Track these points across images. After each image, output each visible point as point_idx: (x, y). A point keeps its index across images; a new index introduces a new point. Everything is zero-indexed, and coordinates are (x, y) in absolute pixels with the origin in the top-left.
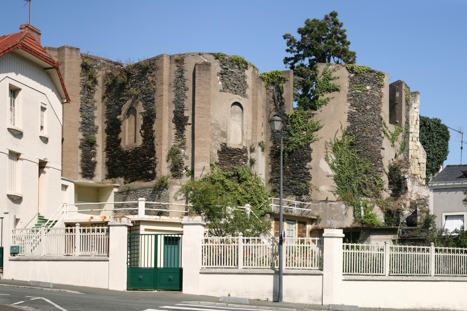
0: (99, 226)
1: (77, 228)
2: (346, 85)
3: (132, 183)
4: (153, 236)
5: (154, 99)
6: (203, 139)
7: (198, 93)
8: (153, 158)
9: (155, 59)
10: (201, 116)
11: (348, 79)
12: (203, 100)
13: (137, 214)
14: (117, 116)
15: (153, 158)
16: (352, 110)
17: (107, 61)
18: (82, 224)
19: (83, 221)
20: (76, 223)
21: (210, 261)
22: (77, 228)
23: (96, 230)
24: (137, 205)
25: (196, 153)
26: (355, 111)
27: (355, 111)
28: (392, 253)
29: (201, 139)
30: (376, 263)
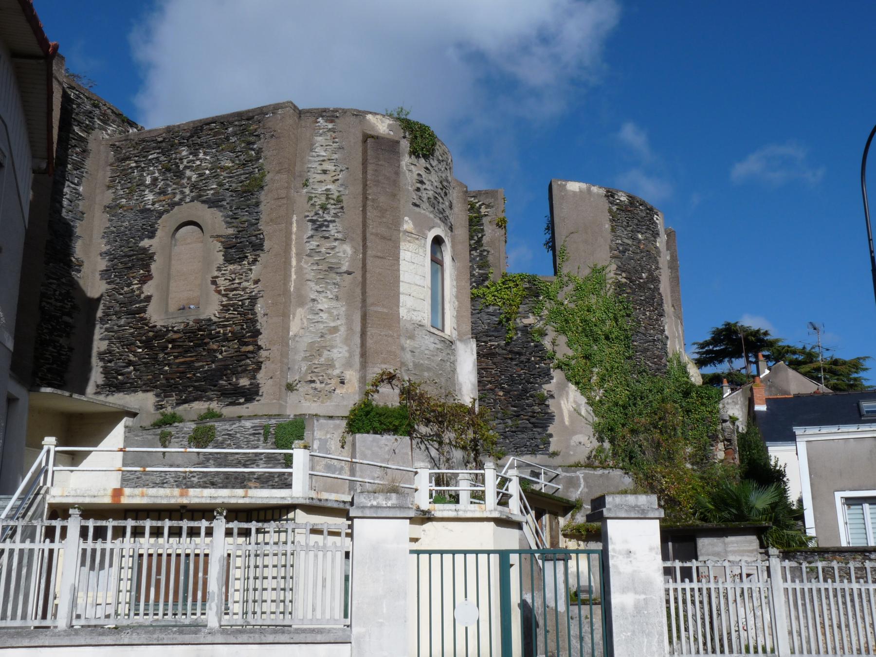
0: (249, 521)
1: (74, 524)
2: (607, 226)
3: (181, 408)
4: (495, 559)
5: (257, 204)
6: (385, 310)
7: (373, 200)
8: (251, 348)
9: (262, 112)
10: (379, 254)
11: (608, 216)
12: (384, 220)
13: (289, 486)
14: (142, 239)
15: (251, 348)
16: (619, 277)
17: (113, 112)
18: (88, 511)
19: (87, 500)
20: (72, 506)
21: (712, 639)
22: (74, 524)
23: (235, 531)
24: (288, 461)
25: (370, 342)
26: (624, 280)
27: (624, 280)
28: (83, 546)
29: (379, 309)
30: (677, 609)
